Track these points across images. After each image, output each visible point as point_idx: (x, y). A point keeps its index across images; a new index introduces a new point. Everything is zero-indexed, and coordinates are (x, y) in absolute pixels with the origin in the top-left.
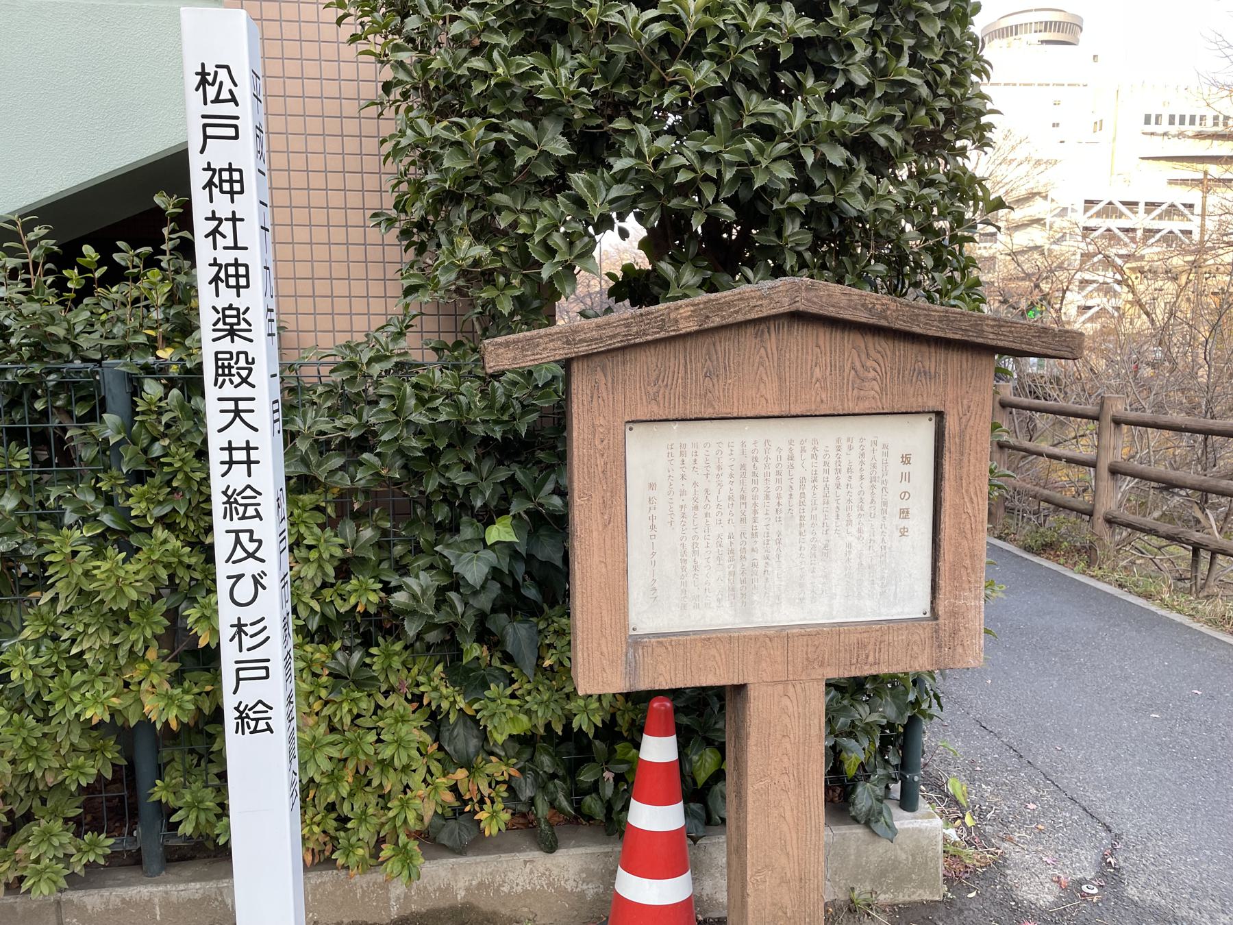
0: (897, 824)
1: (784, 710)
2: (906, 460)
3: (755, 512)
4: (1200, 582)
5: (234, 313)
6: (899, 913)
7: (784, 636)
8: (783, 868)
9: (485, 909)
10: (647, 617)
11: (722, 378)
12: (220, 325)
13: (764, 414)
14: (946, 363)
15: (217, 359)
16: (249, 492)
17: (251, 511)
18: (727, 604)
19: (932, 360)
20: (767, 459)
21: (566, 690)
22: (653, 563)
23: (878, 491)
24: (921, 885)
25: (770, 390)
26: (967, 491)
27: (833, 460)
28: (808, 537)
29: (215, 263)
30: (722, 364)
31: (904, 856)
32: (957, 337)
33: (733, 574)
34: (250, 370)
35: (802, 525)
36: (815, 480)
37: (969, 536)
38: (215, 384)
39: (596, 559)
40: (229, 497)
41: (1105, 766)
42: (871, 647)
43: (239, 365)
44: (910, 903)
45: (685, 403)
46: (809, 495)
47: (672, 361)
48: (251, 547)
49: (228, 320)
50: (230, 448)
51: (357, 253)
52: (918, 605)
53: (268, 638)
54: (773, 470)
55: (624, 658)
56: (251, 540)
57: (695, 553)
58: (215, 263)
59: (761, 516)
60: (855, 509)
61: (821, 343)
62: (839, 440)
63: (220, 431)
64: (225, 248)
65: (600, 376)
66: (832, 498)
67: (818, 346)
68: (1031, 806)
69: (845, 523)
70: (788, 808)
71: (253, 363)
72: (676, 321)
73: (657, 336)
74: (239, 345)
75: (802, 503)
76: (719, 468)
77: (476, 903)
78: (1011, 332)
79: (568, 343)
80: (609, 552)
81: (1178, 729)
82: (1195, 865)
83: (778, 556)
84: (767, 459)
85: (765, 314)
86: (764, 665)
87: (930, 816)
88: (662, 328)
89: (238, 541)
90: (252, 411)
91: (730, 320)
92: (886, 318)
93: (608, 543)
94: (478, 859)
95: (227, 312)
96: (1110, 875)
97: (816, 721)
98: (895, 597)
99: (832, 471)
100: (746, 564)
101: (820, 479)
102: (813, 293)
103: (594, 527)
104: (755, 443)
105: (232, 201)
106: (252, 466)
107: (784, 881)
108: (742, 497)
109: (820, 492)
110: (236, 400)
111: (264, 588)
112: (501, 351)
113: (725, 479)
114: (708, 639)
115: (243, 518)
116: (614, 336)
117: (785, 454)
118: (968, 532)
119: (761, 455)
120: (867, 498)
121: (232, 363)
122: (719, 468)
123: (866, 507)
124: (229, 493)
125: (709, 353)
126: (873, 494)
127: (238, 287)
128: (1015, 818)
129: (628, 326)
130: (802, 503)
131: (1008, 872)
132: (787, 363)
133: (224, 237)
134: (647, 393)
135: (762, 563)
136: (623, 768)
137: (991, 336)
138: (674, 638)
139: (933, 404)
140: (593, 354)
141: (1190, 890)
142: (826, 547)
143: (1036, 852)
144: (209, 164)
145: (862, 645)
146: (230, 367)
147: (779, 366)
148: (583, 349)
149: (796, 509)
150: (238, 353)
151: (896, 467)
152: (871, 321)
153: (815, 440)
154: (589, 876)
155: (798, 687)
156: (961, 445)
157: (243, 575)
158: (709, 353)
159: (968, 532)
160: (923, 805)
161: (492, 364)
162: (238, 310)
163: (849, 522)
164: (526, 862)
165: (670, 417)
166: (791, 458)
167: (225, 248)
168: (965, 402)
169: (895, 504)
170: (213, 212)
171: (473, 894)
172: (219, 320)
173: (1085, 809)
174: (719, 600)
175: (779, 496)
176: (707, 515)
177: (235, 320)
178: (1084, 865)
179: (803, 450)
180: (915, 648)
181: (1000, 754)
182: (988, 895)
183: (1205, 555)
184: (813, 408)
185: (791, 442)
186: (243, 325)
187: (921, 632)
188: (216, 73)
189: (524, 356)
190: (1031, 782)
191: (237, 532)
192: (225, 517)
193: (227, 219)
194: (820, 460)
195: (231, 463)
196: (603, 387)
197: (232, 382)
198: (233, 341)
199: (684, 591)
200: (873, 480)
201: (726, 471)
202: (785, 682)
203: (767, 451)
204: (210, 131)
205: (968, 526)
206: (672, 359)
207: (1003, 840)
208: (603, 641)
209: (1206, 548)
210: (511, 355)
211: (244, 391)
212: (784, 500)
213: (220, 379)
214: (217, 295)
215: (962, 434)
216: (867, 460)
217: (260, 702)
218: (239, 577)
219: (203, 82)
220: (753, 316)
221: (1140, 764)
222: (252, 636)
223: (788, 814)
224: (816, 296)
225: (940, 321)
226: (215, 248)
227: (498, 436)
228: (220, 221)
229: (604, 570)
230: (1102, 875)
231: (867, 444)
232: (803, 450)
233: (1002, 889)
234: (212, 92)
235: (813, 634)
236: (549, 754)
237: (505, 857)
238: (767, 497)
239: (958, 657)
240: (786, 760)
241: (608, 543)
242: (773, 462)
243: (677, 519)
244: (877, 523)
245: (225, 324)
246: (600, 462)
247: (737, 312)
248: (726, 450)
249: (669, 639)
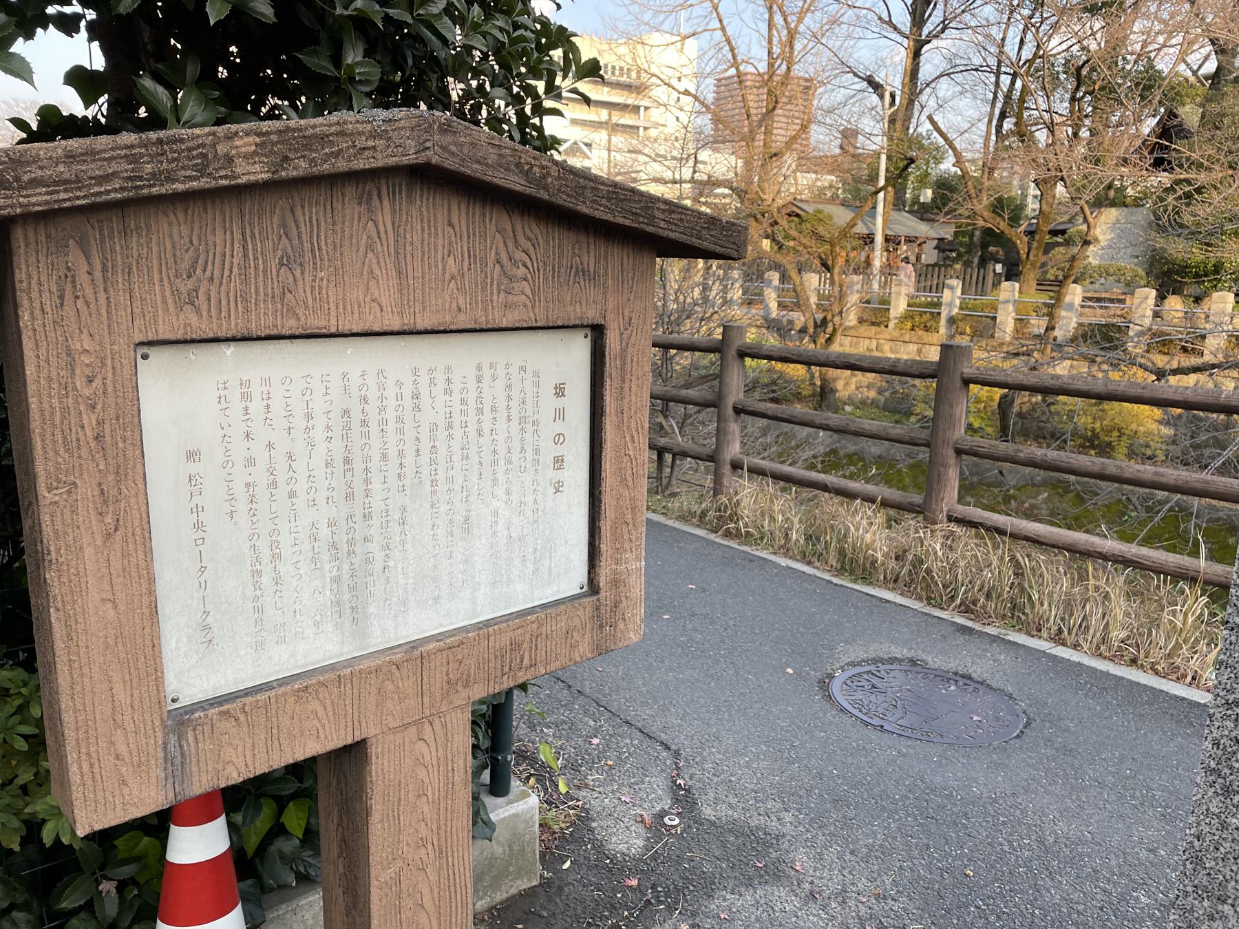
0: (493, 817)
1: (419, 761)
2: (560, 391)
3: (367, 482)
4: (665, 482)
6: (499, 917)
7: (414, 656)
10: (193, 672)
11: (309, 267)
13: (377, 328)
14: (606, 259)
18: (330, 627)
19: (592, 254)
20: (382, 398)
21: (20, 781)
22: (202, 586)
23: (528, 436)
24: (518, 876)
25: (386, 290)
26: (628, 427)
27: (472, 395)
28: (444, 508)
30: (307, 245)
31: (500, 850)
32: (627, 223)
33: (337, 580)
35: (434, 493)
36: (450, 426)
37: (631, 484)
39: (94, 596)
41: (644, 678)
42: (525, 645)
44: (508, 899)
46: (442, 449)
47: (222, 236)
52: (573, 579)
54: (391, 416)
55: (161, 754)
57: (275, 557)
59: (376, 486)
60: (502, 462)
61: (455, 220)
62: (479, 367)
65: (75, 256)
66: (473, 449)
67: (450, 224)
68: (595, 741)
69: (489, 483)
70: (426, 891)
72: (230, 160)
73: (195, 184)
75: (433, 462)
76: (309, 417)
78: (681, 220)
80: (116, 581)
81: (689, 626)
82: (748, 765)
83: (403, 542)
84: (382, 398)
85: (380, 164)
86: (390, 704)
87: (525, 795)
88: (202, 171)
91: (326, 168)
92: (546, 188)
93: (116, 564)
96: (684, 799)
97: (461, 762)
98: (550, 574)
99: (472, 412)
100: (356, 561)
101: (456, 424)
102: (449, 138)
103: (85, 541)
104: (364, 374)
108: (347, 461)
109: (456, 444)
113: (319, 434)
114: (303, 685)
117: (407, 390)
118: (629, 479)
119: (373, 393)
120: (516, 445)
122: (309, 417)
123: (514, 459)
125: (284, 225)
126: (523, 440)
128: (583, 759)
130: (433, 462)
131: (594, 825)
132: (409, 248)
134: (175, 291)
136: (127, 871)
137: (662, 224)
139: (592, 315)
140: (61, 210)
141: (753, 795)
142: (466, 519)
143: (613, 792)
145: (516, 645)
147: (397, 253)
148: (38, 199)
149: (426, 471)
151: (549, 402)
152: (528, 191)
155: (437, 724)
156: (623, 368)
158: (284, 225)
159: (629, 479)
160: (515, 784)
163: (495, 482)
165: (222, 334)
166: (416, 396)
168: (626, 314)
169: (549, 451)
173: (641, 731)
174: (316, 624)
175: (401, 454)
176: (292, 494)
178: (656, 795)
179: (432, 383)
180: (575, 634)
181: (551, 689)
182: (582, 860)
183: (668, 457)
184: (447, 320)
185: (415, 372)
187: (581, 613)
190: (586, 712)
194: (456, 397)
196: (83, 278)
200: (522, 420)
201: (320, 421)
202: (418, 723)
203: (381, 387)
205: (629, 472)
206: (219, 232)
207: (579, 788)
209: (669, 450)
212: (409, 459)
215: (623, 352)
216: (515, 394)
220: (361, 164)
221: (671, 669)
224: (456, 144)
225: (609, 199)
229: (112, 613)
230: (676, 800)
231: (514, 370)
232: (432, 383)
233: (594, 848)
235: (453, 644)
238: (384, 456)
239: (619, 635)
241: (116, 564)
242: (391, 403)
243: (242, 506)
244: (528, 478)
246: (89, 419)
247: (336, 155)
248: (319, 388)
249: (238, 704)
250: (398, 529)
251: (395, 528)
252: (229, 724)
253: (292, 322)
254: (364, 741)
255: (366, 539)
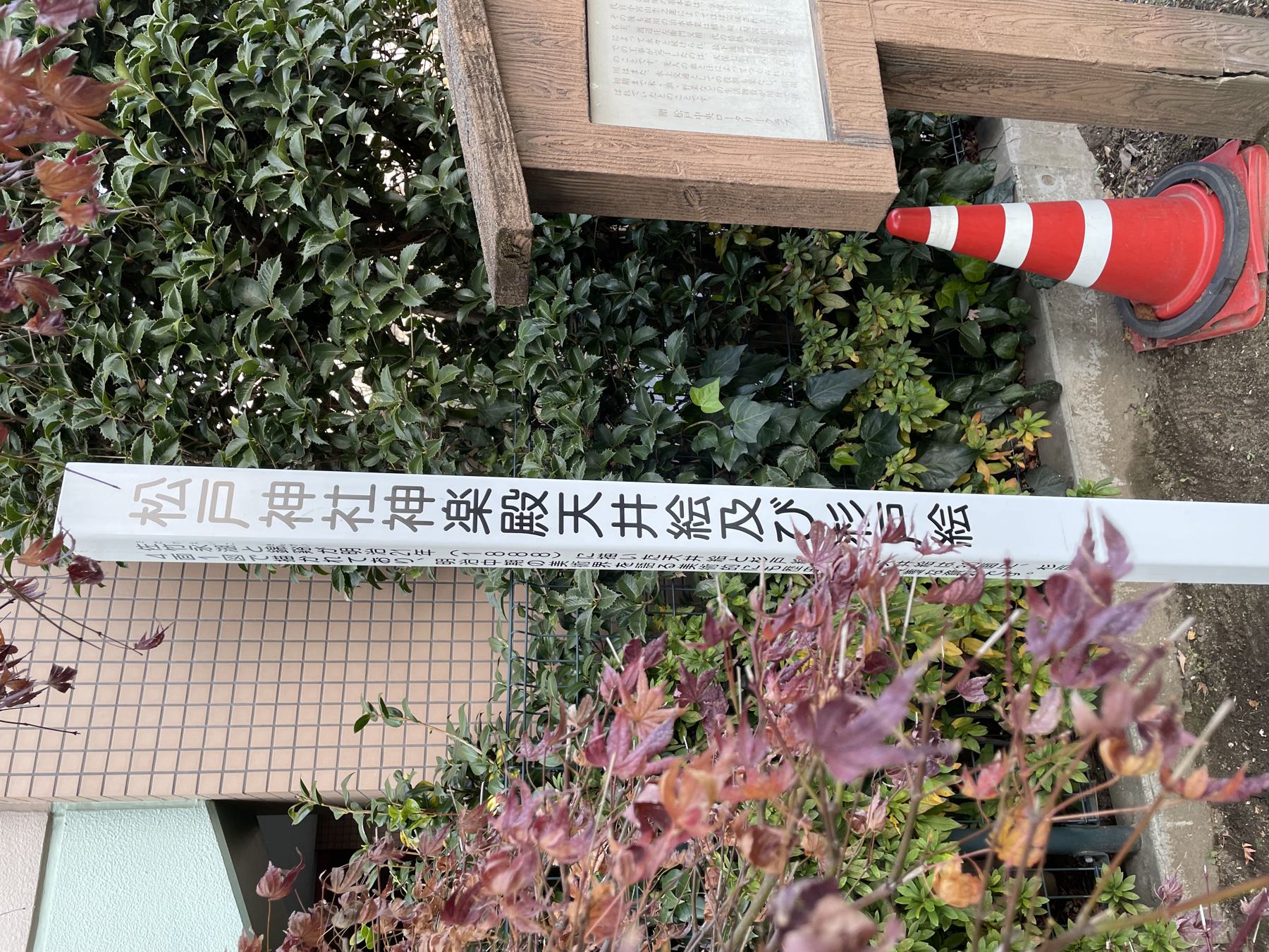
3: (689, 24)
5: (454, 507)
8: (1066, 29)
9: (1131, 457)
12: (470, 523)
15: (512, 530)
16: (676, 509)
17: (699, 509)
18: (790, 58)
29: (390, 522)
33: (757, 50)
34: (525, 495)
38: (543, 535)
39: (746, 163)
40: (682, 531)
43: (519, 507)
45: (570, 67)
48: (742, 513)
49: (463, 514)
50: (622, 525)
51: (379, 652)
53: (852, 502)
56: (734, 511)
58: (390, 522)
59: (693, 20)
63: (600, 535)
64: (371, 509)
71: (517, 492)
73: (494, 64)
74: (494, 504)
77: (1126, 467)
79: (500, 148)
83: (736, 9)
86: (853, 24)
88: (485, 60)
89: (736, 526)
90: (576, 498)
94: (1076, 463)
95: (453, 514)
105: (313, 496)
106: (643, 503)
107: (1079, 29)
108: (673, 33)
110: (562, 514)
111: (791, 502)
112: (508, 213)
115: (707, 517)
116: (494, 104)
121: (516, 514)
122: (641, 51)
124: (677, 530)
127: (422, 500)
129: (482, 90)
133: (357, 509)
135: (744, 24)
138: (830, 101)
144: (262, 519)
146: (521, 517)
150: (504, 506)
153: (612, 6)
154: (1081, 352)
157: (777, 524)
158: (516, 40)
161: (523, 223)
162: (450, 503)
164: (1074, 414)
167: (371, 509)
170: (324, 519)
171: (1115, 469)
172: (462, 524)
176: (693, 67)
177: (463, 507)
186: (470, 497)
188: (145, 501)
189: (514, 191)
191: (724, 526)
192: (707, 538)
193: (335, 504)
195: (639, 526)
196: (550, 139)
197: (539, 517)
198: (489, 511)
199: (778, 94)
201: (645, 45)
204: (220, 513)
208: (838, 165)
210: (513, 203)
211: (551, 503)
213: (536, 529)
214: (431, 523)
217: (930, 517)
218: (779, 528)
219: (157, 517)
222: (851, 520)
223: (1012, 19)
226: (371, 521)
227: (599, 390)
228: (336, 512)
234: (168, 508)
236: (953, 386)
237: (1071, 436)
240: (953, 15)
243: (699, 94)
245: (467, 518)
250: (726, 10)
251: (724, 12)
252: (845, 114)
253: (578, 45)
254: (877, 44)
255: (731, 30)
